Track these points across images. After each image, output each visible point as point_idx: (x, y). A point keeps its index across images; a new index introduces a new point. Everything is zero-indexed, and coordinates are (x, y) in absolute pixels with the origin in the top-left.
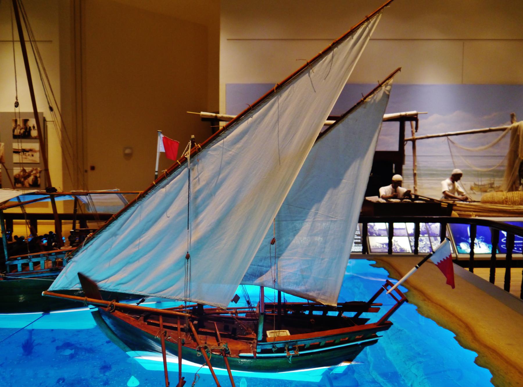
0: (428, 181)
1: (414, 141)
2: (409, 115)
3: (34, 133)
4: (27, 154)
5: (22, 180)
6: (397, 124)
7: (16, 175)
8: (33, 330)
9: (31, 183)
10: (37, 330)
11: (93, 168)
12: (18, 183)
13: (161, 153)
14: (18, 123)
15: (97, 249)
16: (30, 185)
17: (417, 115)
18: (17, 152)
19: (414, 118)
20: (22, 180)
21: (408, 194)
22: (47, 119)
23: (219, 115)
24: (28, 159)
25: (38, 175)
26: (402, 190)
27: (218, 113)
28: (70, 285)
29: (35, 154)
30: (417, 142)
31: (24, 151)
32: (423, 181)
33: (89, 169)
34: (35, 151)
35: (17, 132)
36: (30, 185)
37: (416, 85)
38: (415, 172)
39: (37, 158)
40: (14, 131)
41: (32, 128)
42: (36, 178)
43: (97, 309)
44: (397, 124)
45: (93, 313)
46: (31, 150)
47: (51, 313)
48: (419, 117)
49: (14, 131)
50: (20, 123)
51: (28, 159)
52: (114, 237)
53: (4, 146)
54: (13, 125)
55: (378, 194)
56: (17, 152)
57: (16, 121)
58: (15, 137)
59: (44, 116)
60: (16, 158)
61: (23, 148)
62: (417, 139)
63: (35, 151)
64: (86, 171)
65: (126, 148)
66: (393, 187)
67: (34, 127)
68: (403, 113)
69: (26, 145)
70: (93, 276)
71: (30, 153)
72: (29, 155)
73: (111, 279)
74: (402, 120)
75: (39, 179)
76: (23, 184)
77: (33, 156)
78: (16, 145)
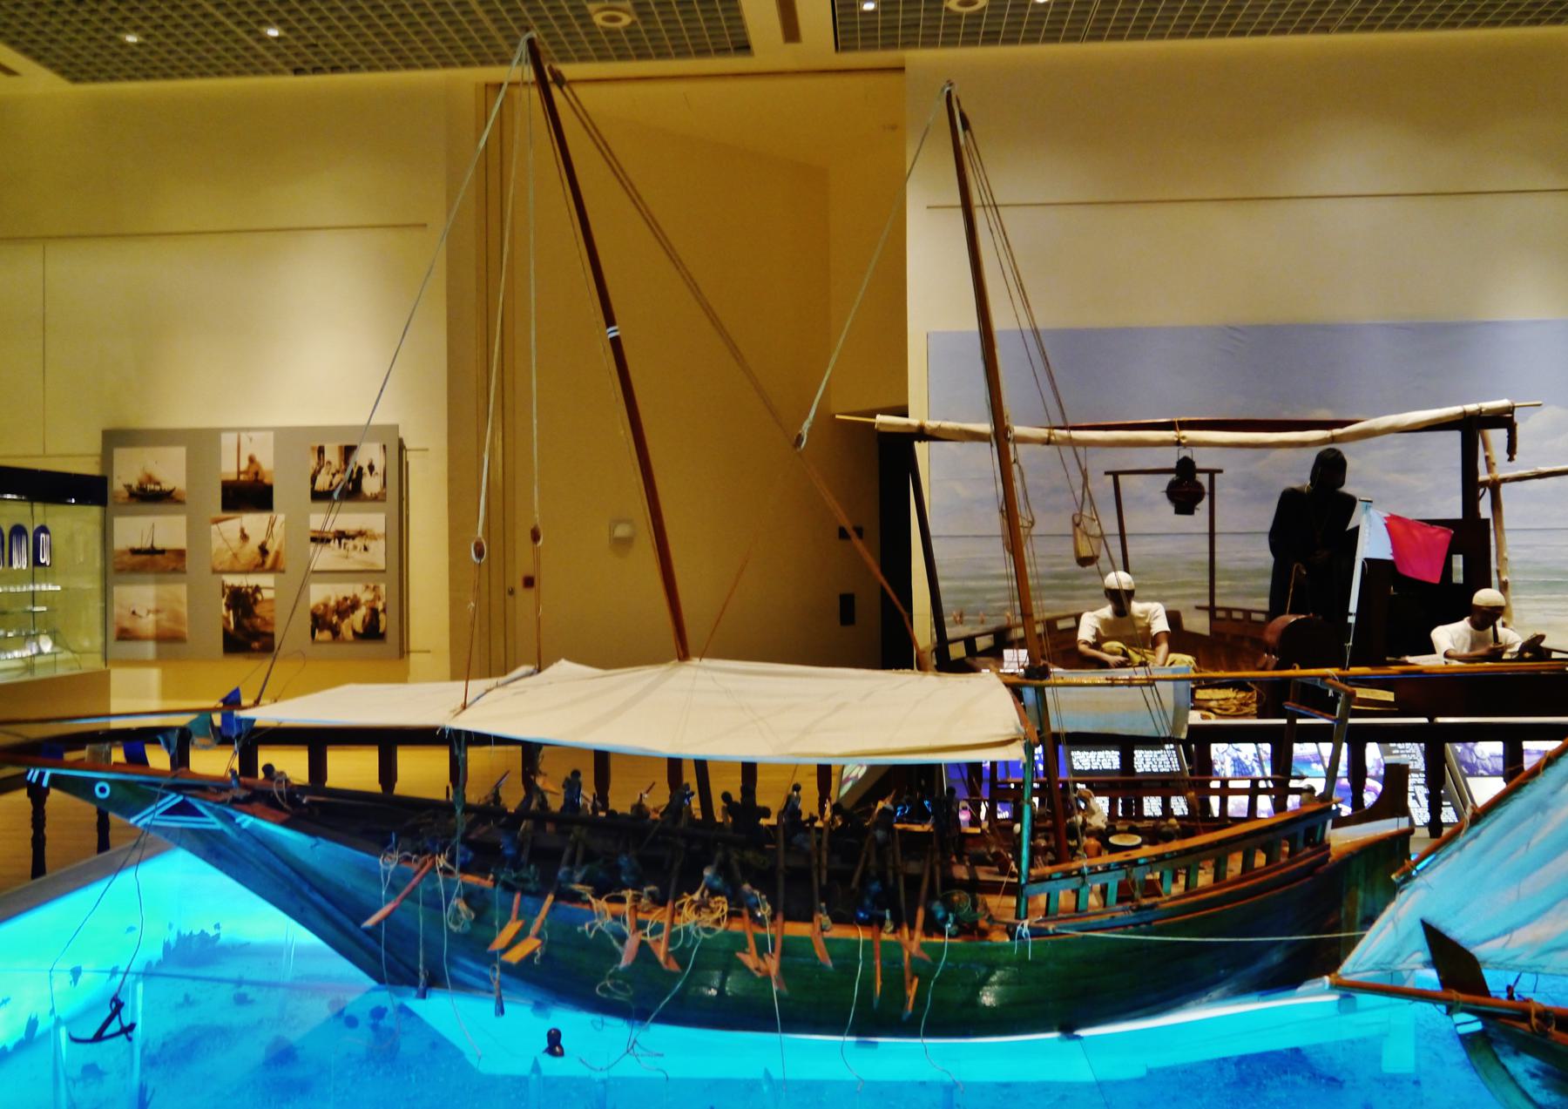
0: (1538, 606)
1: (1494, 486)
2: (1488, 411)
3: (371, 485)
4: (350, 543)
5: (335, 619)
6: (1455, 437)
7: (317, 606)
8: (956, 1084)
9: (359, 628)
10: (965, 1085)
11: (529, 582)
12: (321, 630)
13: (1370, 563)
14: (328, 456)
15: (1485, 850)
16: (355, 633)
17: (1511, 410)
18: (320, 539)
19: (1503, 419)
20: (335, 619)
21: (1534, 647)
22: (408, 444)
23: (913, 420)
24: (354, 557)
25: (380, 606)
26: (1512, 636)
27: (904, 413)
28: (1398, 955)
29: (372, 545)
30: (1504, 488)
31: (341, 536)
32: (1523, 606)
33: (519, 584)
34: (374, 537)
35: (323, 482)
36: (355, 633)
37: (1496, 324)
38: (1504, 578)
39: (377, 555)
40: (314, 480)
41: (366, 470)
42: (374, 613)
43: (1478, 1026)
44: (1455, 437)
45: (1468, 1041)
46: (361, 534)
47: (1083, 1033)
48: (1518, 416)
49: (314, 480)
50: (333, 455)
51: (354, 557)
52: (1539, 815)
53: (286, 521)
54: (313, 462)
55: (1429, 649)
56: (320, 539)
57: (321, 451)
58: (317, 496)
59: (401, 435)
60: (326, 557)
61: (341, 527)
62: (1504, 480)
63: (374, 537)
64: (512, 592)
65: (619, 521)
66: (1474, 624)
67: (371, 468)
68: (1471, 407)
69: (348, 518)
70: (1458, 931)
71: (359, 542)
72: (355, 547)
73: (1523, 936)
74: (1471, 427)
75: (382, 617)
76: (336, 632)
77: (366, 549)
78: (319, 519)
